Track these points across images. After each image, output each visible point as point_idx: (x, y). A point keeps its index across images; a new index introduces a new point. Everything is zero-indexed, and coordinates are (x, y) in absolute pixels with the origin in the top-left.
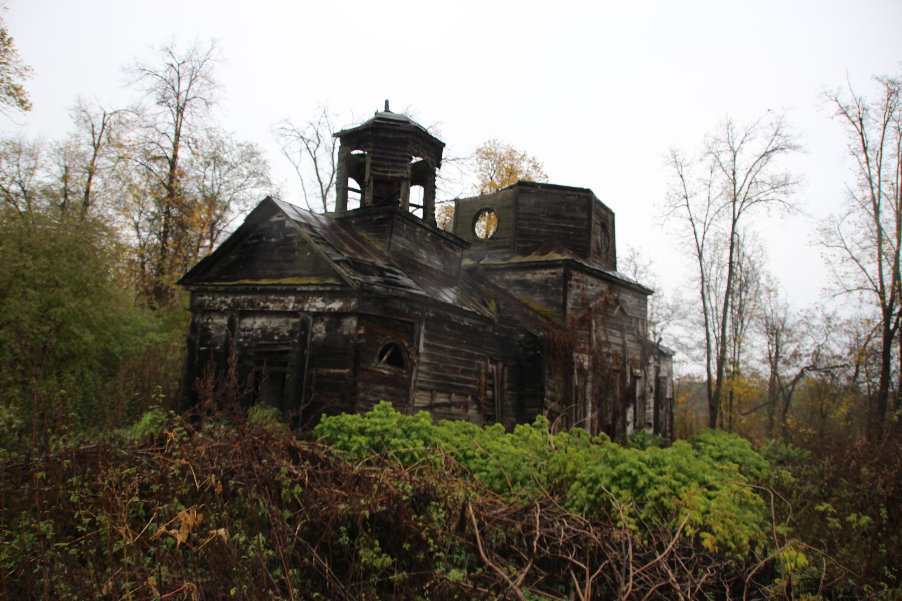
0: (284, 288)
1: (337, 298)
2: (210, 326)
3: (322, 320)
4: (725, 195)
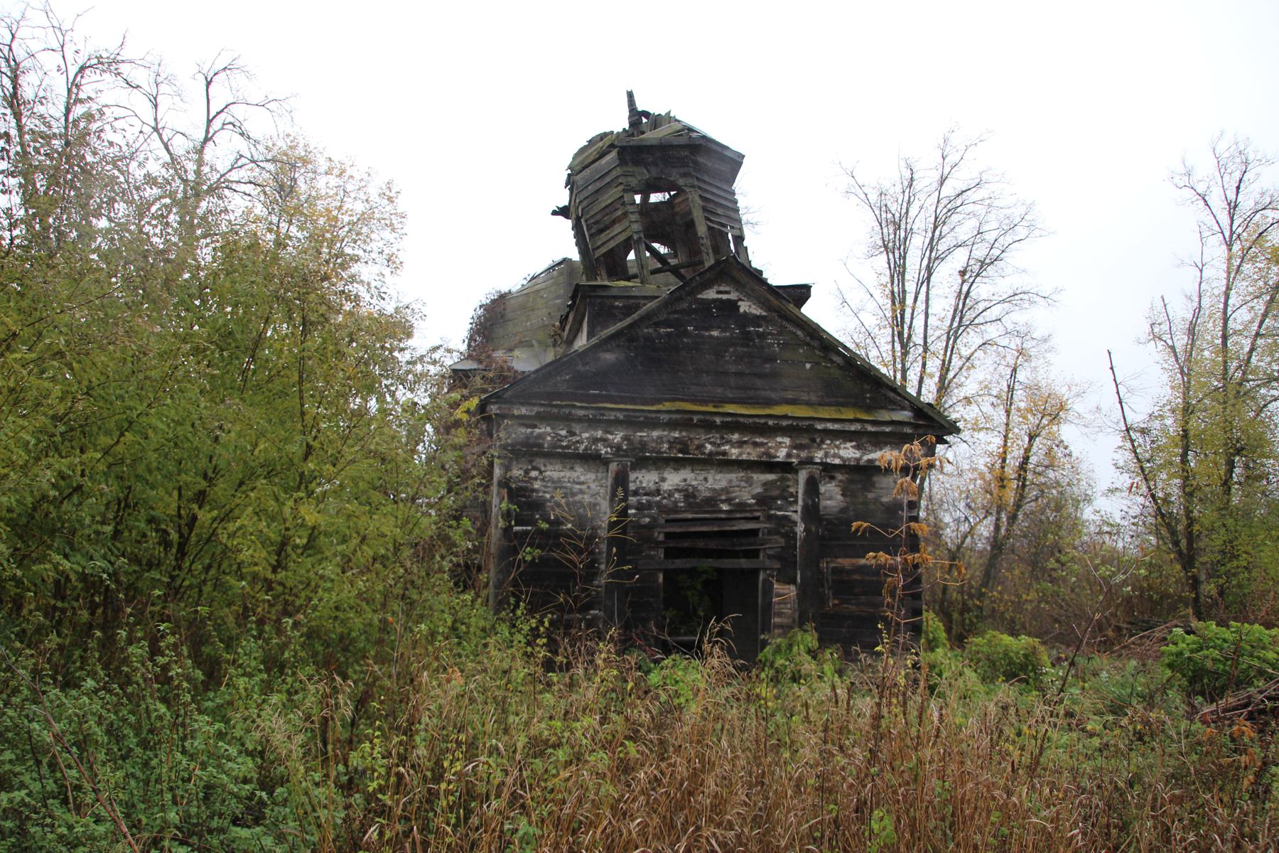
0: (784, 423)
1: (886, 444)
2: (537, 485)
3: (832, 478)
4: (859, 338)
